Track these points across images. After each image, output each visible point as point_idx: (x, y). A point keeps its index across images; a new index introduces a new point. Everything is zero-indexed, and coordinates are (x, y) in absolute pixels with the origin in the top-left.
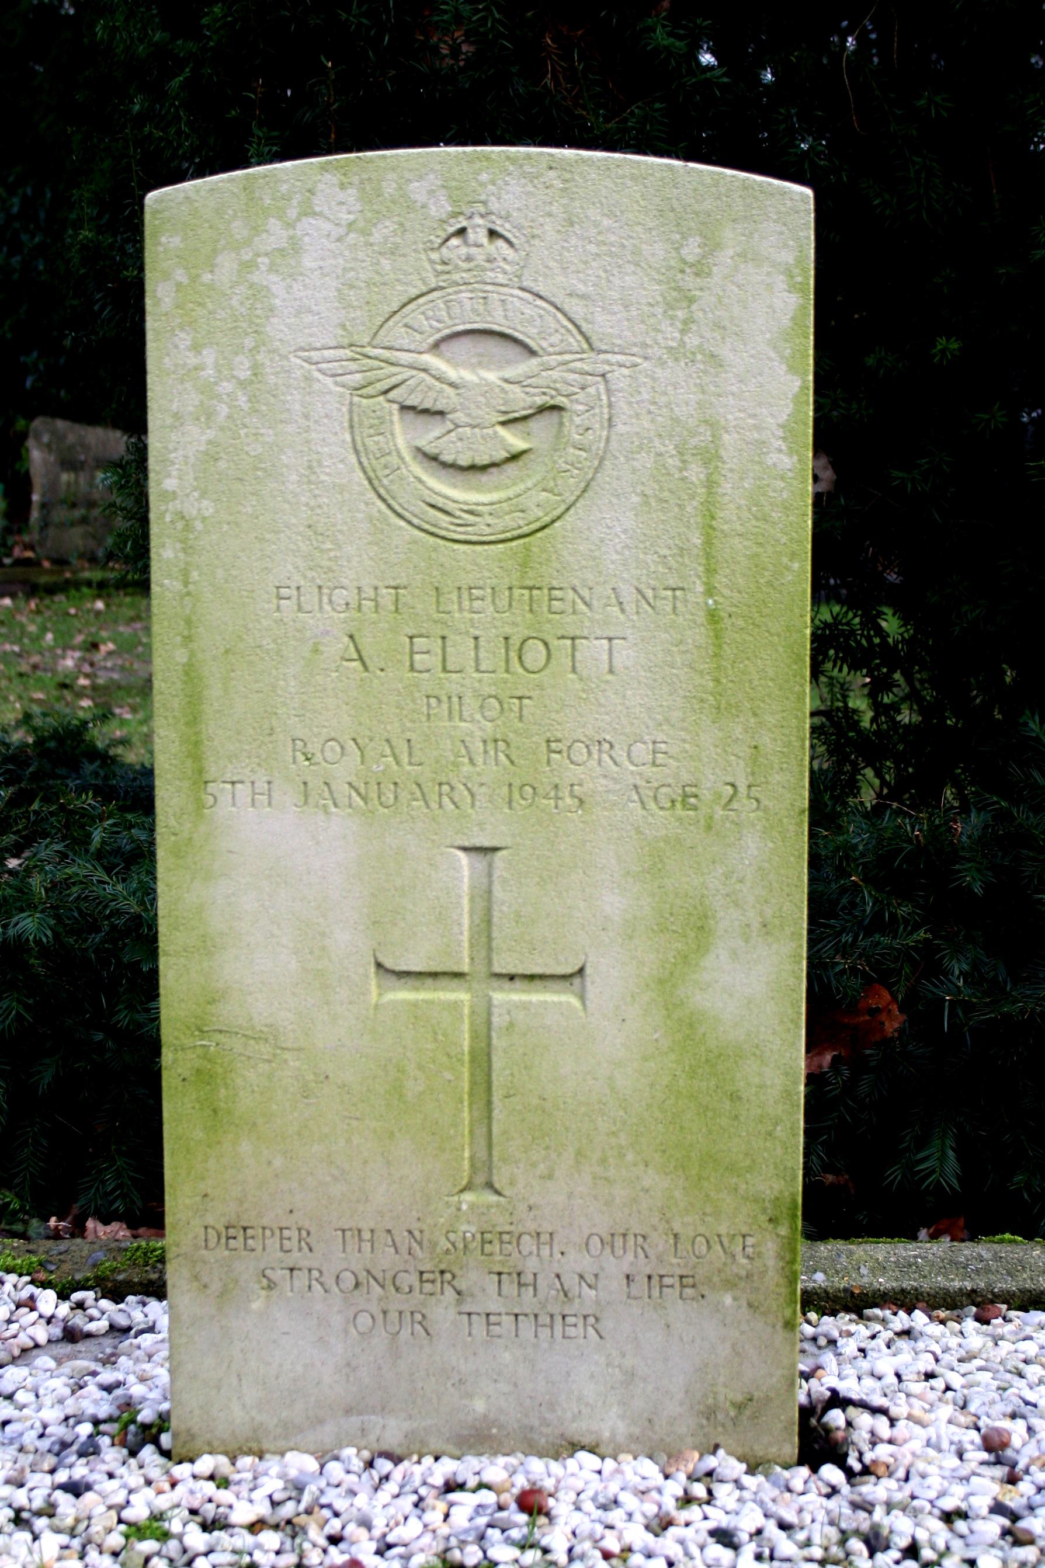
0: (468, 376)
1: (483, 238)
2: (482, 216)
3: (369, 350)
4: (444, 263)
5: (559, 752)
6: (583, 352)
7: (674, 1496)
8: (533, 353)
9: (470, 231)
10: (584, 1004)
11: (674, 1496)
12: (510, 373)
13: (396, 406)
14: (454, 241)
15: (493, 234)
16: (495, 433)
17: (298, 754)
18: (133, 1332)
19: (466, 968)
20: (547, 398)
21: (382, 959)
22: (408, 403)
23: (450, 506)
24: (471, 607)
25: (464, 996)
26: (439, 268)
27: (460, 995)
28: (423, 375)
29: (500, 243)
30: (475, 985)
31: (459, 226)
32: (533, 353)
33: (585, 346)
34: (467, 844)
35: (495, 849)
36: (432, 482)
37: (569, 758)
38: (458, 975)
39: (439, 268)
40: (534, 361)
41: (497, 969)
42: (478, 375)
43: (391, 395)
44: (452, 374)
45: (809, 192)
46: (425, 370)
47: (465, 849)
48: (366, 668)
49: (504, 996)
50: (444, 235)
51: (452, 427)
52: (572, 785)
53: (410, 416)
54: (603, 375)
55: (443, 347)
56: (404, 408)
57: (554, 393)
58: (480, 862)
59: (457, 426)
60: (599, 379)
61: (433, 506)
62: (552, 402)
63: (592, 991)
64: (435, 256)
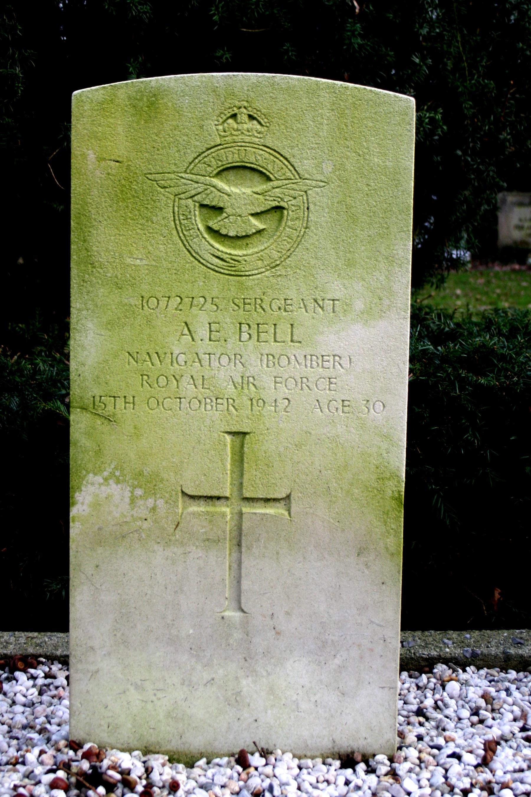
0: (235, 190)
1: (246, 118)
2: (245, 107)
3: (183, 175)
4: (225, 131)
5: (281, 383)
6: (296, 179)
7: (351, 774)
8: (269, 179)
9: (239, 116)
10: (289, 514)
11: (351, 774)
12: (255, 190)
13: (197, 204)
14: (230, 121)
15: (251, 118)
16: (249, 220)
17: (304, 385)
18: (186, 730)
19: (228, 495)
20: (276, 202)
21: (184, 490)
22: (205, 203)
23: (225, 256)
24: (285, 309)
25: (228, 510)
26: (223, 134)
27: (225, 509)
28: (212, 189)
29: (255, 122)
30: (232, 503)
31: (233, 113)
32: (269, 179)
33: (297, 177)
34: (234, 430)
35: (245, 434)
36: (217, 245)
37: (286, 386)
38: (227, 498)
39: (223, 134)
40: (271, 183)
41: (247, 495)
42: (241, 190)
43: (196, 198)
44: (226, 188)
45: (413, 99)
46: (214, 187)
47: (229, 433)
48: (193, 340)
49: (247, 509)
50: (225, 118)
51: (227, 216)
52: (101, 397)
53: (205, 211)
54: (306, 192)
55: (225, 174)
56: (202, 206)
57: (279, 200)
58: (238, 439)
59: (229, 216)
60: (303, 193)
61: (214, 255)
62: (277, 204)
63: (294, 508)
64: (220, 127)
